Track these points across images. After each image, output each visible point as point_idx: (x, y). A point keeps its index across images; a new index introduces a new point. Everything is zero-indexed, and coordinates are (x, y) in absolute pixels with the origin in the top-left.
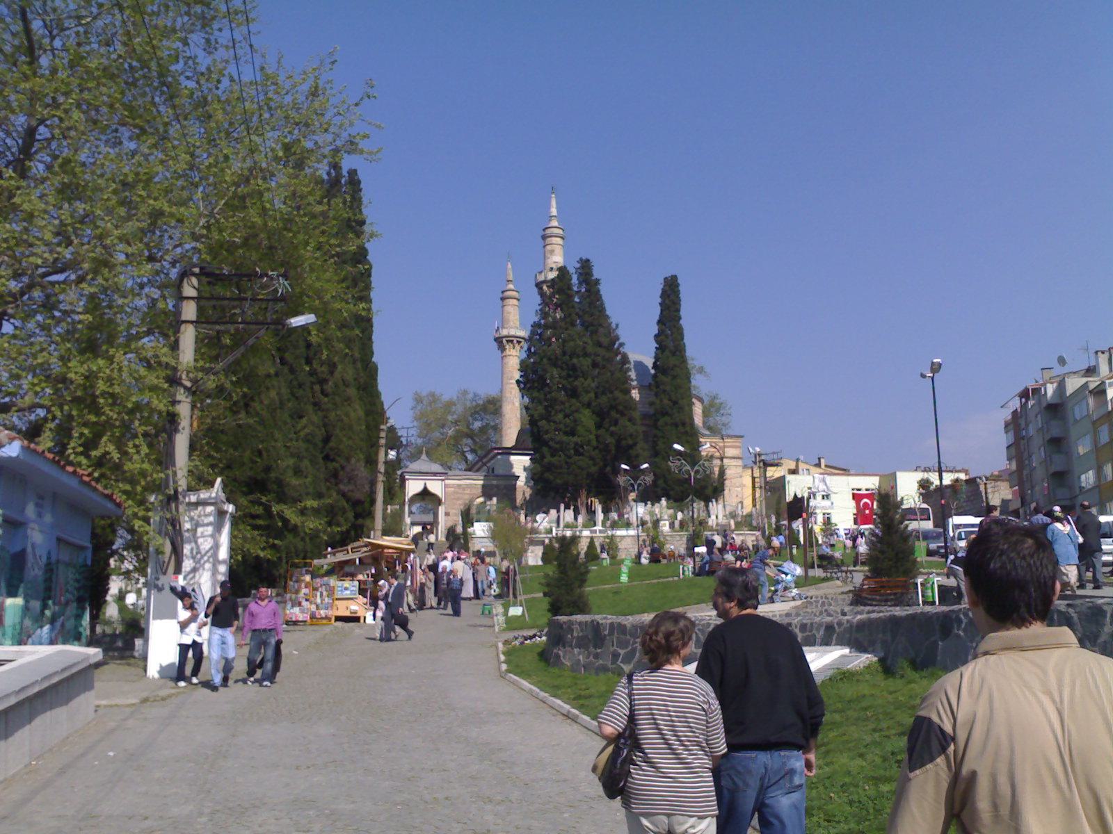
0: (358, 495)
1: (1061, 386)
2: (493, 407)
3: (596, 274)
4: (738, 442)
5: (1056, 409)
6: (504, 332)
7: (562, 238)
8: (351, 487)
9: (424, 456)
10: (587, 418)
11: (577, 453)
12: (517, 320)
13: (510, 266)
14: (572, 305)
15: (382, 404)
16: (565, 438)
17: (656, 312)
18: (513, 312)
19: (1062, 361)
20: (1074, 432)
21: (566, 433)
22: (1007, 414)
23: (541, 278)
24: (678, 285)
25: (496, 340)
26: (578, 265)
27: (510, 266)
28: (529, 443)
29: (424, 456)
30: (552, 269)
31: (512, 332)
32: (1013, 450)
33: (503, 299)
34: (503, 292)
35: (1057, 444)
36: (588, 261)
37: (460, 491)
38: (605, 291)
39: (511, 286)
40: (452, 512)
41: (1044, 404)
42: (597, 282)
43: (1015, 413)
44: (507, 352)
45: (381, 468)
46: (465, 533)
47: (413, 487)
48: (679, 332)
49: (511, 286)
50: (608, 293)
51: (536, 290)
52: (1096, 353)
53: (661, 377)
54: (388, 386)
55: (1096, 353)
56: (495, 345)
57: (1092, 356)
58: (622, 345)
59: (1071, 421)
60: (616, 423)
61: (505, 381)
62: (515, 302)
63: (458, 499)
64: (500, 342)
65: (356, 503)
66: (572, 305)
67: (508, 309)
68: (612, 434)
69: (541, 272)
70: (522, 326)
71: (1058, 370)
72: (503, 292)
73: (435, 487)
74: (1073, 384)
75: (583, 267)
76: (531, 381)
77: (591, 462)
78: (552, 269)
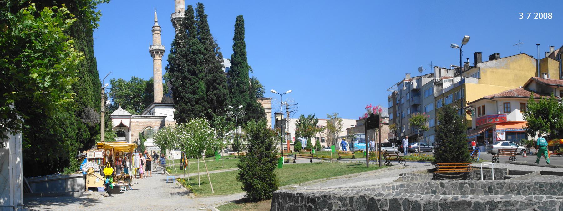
1: (419, 81)
2: (150, 86)
3: (206, 12)
4: (269, 101)
5: (416, 92)
6: (154, 48)
7: (160, 31)
9: (120, 108)
10: (203, 85)
11: (197, 103)
12: (162, 41)
13: (156, 14)
14: (193, 26)
15: (35, 205)
16: (191, 96)
17: (232, 34)
18: (157, 37)
19: (420, 70)
20: (424, 102)
21: (191, 93)
22: (390, 94)
23: (174, 17)
25: (150, 52)
27: (156, 14)
28: (170, 100)
29: (120, 108)
30: (179, 12)
31: (158, 48)
32: (392, 109)
33: (153, 31)
34: (153, 27)
35: (416, 108)
36: (202, 4)
37: (138, 124)
38: (209, 21)
39: (157, 24)
40: (134, 134)
41: (411, 89)
42: (206, 16)
43: (394, 93)
44: (156, 58)
45: (103, 109)
46: (142, 144)
47: (116, 123)
49: (157, 24)
50: (211, 22)
51: (171, 23)
52: (435, 67)
53: (235, 68)
54: (101, 76)
55: (435, 67)
56: (150, 54)
57: (433, 69)
58: (218, 48)
59: (423, 97)
61: (155, 72)
62: (159, 32)
63: (137, 128)
64: (153, 53)
65: (91, 129)
66: (193, 26)
67: (155, 36)
70: (163, 44)
71: (420, 74)
72: (153, 27)
73: (126, 122)
74: (425, 81)
75: (199, 8)
76: (173, 68)
77: (204, 108)
78: (179, 12)
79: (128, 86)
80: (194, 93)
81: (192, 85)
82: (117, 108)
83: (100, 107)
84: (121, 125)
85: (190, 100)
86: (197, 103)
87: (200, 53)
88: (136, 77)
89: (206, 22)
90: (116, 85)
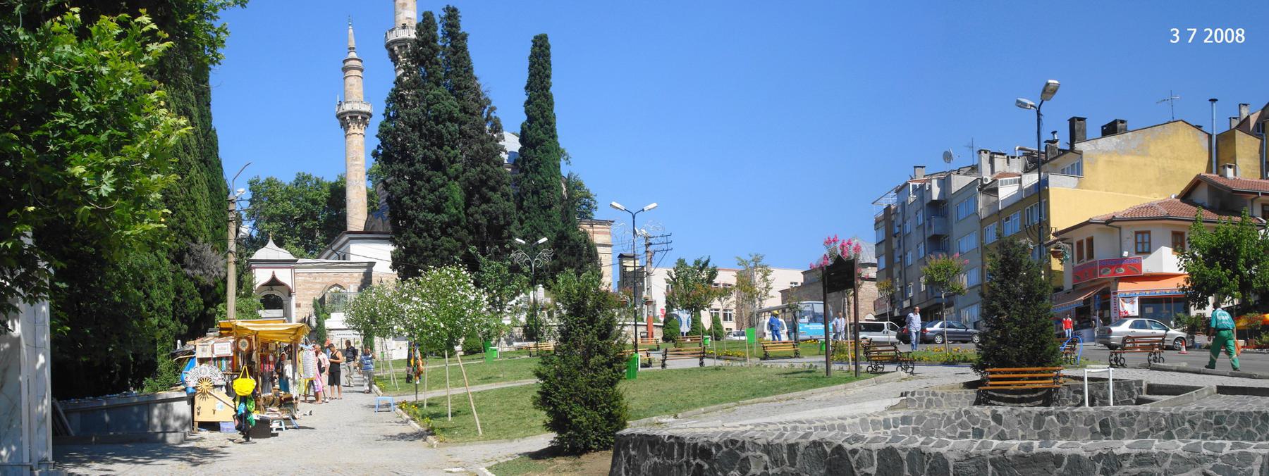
0: (207, 281)
1: (945, 182)
2: (338, 195)
3: (464, 27)
5: (938, 208)
6: (347, 108)
8: (198, 272)
9: (271, 244)
10: (457, 192)
11: (444, 232)
12: (366, 91)
13: (351, 31)
14: (435, 59)
16: (430, 216)
17: (523, 77)
19: (948, 157)
20: (957, 230)
21: (431, 211)
22: (878, 211)
23: (392, 37)
24: (548, 48)
25: (338, 116)
26: (443, 14)
27: (351, 31)
28: (383, 224)
29: (271, 244)
31: (357, 107)
33: (345, 70)
34: (345, 62)
35: (938, 243)
36: (455, 10)
37: (311, 280)
39: (353, 55)
40: (303, 303)
41: (927, 201)
42: (464, 37)
43: (888, 209)
44: (351, 130)
45: (232, 246)
47: (261, 276)
48: (549, 99)
49: (353, 55)
50: (475, 49)
51: (387, 52)
54: (229, 172)
56: (338, 122)
57: (976, 155)
58: (492, 109)
59: (955, 219)
60: (487, 200)
61: (349, 162)
62: (358, 73)
64: (346, 120)
66: (435, 59)
68: (484, 213)
69: (391, 30)
70: (367, 99)
72: (345, 62)
73: (284, 275)
74: (959, 182)
75: (449, 17)
76: (390, 153)
77: (459, 244)
79: (290, 195)
80: (437, 210)
81: (432, 191)
82: (264, 244)
83: (224, 241)
84: (274, 282)
85: (429, 226)
86: (444, 232)
87: (452, 119)
88: (307, 173)
89: (464, 49)
90: (262, 192)
